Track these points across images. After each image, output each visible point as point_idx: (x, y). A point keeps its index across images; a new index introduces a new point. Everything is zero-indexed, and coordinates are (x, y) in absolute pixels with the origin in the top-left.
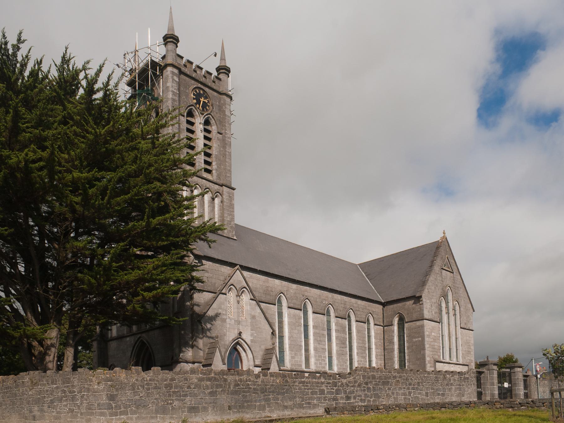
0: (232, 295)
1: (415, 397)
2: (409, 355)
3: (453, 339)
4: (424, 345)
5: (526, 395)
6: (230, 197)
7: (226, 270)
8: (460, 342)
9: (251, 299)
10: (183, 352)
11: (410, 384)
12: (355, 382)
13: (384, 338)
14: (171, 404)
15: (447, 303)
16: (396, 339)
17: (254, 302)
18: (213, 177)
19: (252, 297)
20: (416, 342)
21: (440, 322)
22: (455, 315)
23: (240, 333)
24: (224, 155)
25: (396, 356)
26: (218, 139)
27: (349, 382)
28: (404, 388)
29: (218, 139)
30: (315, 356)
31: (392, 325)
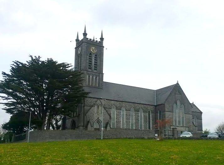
0: (96, 107)
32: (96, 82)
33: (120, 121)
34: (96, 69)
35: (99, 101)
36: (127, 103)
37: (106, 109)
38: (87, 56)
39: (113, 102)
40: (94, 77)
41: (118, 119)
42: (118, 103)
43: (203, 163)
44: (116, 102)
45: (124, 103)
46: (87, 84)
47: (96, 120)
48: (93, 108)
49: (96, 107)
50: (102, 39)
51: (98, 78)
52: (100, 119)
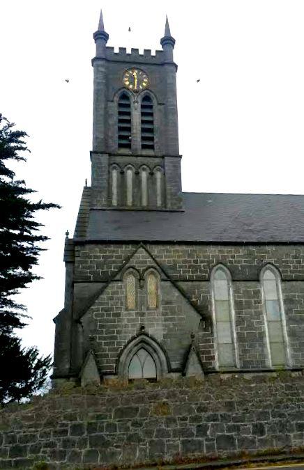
0: (130, 281)
1: (219, 438)
6: (175, 166)
7: (123, 251)
9: (163, 280)
11: (201, 409)
12: (39, 416)
17: (168, 284)
18: (157, 151)
19: (165, 278)
23: (143, 328)
24: (166, 125)
26: (160, 110)
27: (24, 418)
28: (184, 419)
29: (160, 110)
30: (292, 345)
31: (208, 280)
32: (155, 191)
33: (262, 335)
34: (152, 147)
35: (141, 254)
36: (284, 248)
37: (183, 285)
38: (110, 104)
39: (212, 252)
40: (144, 175)
41: (250, 327)
42: (242, 251)
43: (241, 468)
44: (232, 249)
45: (267, 248)
46: (115, 202)
47: (134, 338)
48: (113, 287)
49: (130, 281)
50: (168, 41)
51: (158, 175)
52: (150, 331)
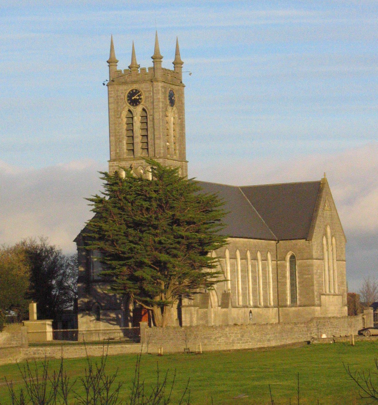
2: (299, 289)
3: (331, 272)
4: (313, 282)
5: (93, 375)
8: (336, 274)
10: (158, 307)
13: (277, 273)
14: (262, 338)
15: (327, 239)
16: (288, 274)
20: (306, 278)
21: (323, 259)
22: (332, 250)
25: (288, 289)
